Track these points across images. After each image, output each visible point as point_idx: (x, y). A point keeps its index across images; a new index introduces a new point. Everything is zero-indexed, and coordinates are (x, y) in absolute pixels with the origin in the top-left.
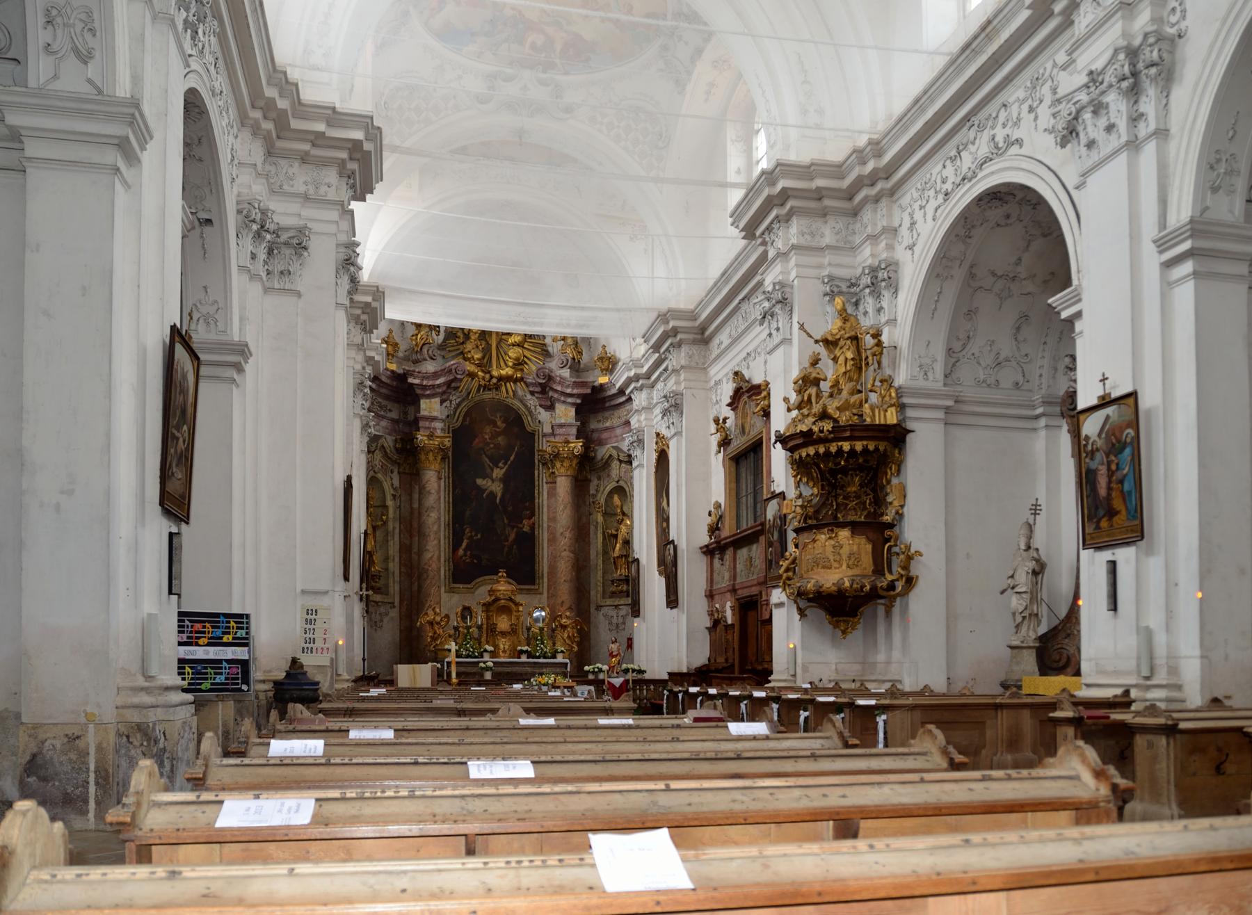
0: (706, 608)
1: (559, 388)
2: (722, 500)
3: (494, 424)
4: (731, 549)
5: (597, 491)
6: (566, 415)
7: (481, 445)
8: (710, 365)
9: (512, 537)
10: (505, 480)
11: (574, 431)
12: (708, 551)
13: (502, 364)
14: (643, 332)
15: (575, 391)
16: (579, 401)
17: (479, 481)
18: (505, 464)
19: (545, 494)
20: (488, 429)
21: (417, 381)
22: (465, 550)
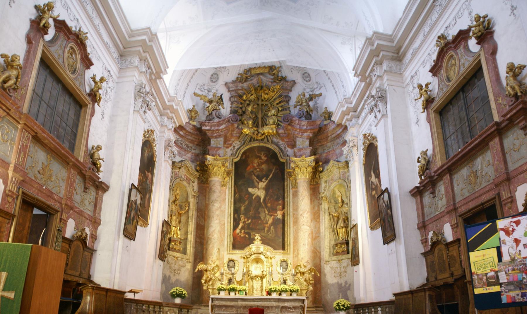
0: (419, 238)
2: (430, 147)
3: (260, 158)
4: (448, 176)
5: (325, 190)
7: (251, 170)
8: (404, 71)
9: (270, 221)
10: (267, 189)
11: (308, 151)
12: (418, 192)
14: (353, 67)
17: (250, 190)
18: (266, 179)
19: (292, 223)
21: (208, 128)
22: (241, 230)
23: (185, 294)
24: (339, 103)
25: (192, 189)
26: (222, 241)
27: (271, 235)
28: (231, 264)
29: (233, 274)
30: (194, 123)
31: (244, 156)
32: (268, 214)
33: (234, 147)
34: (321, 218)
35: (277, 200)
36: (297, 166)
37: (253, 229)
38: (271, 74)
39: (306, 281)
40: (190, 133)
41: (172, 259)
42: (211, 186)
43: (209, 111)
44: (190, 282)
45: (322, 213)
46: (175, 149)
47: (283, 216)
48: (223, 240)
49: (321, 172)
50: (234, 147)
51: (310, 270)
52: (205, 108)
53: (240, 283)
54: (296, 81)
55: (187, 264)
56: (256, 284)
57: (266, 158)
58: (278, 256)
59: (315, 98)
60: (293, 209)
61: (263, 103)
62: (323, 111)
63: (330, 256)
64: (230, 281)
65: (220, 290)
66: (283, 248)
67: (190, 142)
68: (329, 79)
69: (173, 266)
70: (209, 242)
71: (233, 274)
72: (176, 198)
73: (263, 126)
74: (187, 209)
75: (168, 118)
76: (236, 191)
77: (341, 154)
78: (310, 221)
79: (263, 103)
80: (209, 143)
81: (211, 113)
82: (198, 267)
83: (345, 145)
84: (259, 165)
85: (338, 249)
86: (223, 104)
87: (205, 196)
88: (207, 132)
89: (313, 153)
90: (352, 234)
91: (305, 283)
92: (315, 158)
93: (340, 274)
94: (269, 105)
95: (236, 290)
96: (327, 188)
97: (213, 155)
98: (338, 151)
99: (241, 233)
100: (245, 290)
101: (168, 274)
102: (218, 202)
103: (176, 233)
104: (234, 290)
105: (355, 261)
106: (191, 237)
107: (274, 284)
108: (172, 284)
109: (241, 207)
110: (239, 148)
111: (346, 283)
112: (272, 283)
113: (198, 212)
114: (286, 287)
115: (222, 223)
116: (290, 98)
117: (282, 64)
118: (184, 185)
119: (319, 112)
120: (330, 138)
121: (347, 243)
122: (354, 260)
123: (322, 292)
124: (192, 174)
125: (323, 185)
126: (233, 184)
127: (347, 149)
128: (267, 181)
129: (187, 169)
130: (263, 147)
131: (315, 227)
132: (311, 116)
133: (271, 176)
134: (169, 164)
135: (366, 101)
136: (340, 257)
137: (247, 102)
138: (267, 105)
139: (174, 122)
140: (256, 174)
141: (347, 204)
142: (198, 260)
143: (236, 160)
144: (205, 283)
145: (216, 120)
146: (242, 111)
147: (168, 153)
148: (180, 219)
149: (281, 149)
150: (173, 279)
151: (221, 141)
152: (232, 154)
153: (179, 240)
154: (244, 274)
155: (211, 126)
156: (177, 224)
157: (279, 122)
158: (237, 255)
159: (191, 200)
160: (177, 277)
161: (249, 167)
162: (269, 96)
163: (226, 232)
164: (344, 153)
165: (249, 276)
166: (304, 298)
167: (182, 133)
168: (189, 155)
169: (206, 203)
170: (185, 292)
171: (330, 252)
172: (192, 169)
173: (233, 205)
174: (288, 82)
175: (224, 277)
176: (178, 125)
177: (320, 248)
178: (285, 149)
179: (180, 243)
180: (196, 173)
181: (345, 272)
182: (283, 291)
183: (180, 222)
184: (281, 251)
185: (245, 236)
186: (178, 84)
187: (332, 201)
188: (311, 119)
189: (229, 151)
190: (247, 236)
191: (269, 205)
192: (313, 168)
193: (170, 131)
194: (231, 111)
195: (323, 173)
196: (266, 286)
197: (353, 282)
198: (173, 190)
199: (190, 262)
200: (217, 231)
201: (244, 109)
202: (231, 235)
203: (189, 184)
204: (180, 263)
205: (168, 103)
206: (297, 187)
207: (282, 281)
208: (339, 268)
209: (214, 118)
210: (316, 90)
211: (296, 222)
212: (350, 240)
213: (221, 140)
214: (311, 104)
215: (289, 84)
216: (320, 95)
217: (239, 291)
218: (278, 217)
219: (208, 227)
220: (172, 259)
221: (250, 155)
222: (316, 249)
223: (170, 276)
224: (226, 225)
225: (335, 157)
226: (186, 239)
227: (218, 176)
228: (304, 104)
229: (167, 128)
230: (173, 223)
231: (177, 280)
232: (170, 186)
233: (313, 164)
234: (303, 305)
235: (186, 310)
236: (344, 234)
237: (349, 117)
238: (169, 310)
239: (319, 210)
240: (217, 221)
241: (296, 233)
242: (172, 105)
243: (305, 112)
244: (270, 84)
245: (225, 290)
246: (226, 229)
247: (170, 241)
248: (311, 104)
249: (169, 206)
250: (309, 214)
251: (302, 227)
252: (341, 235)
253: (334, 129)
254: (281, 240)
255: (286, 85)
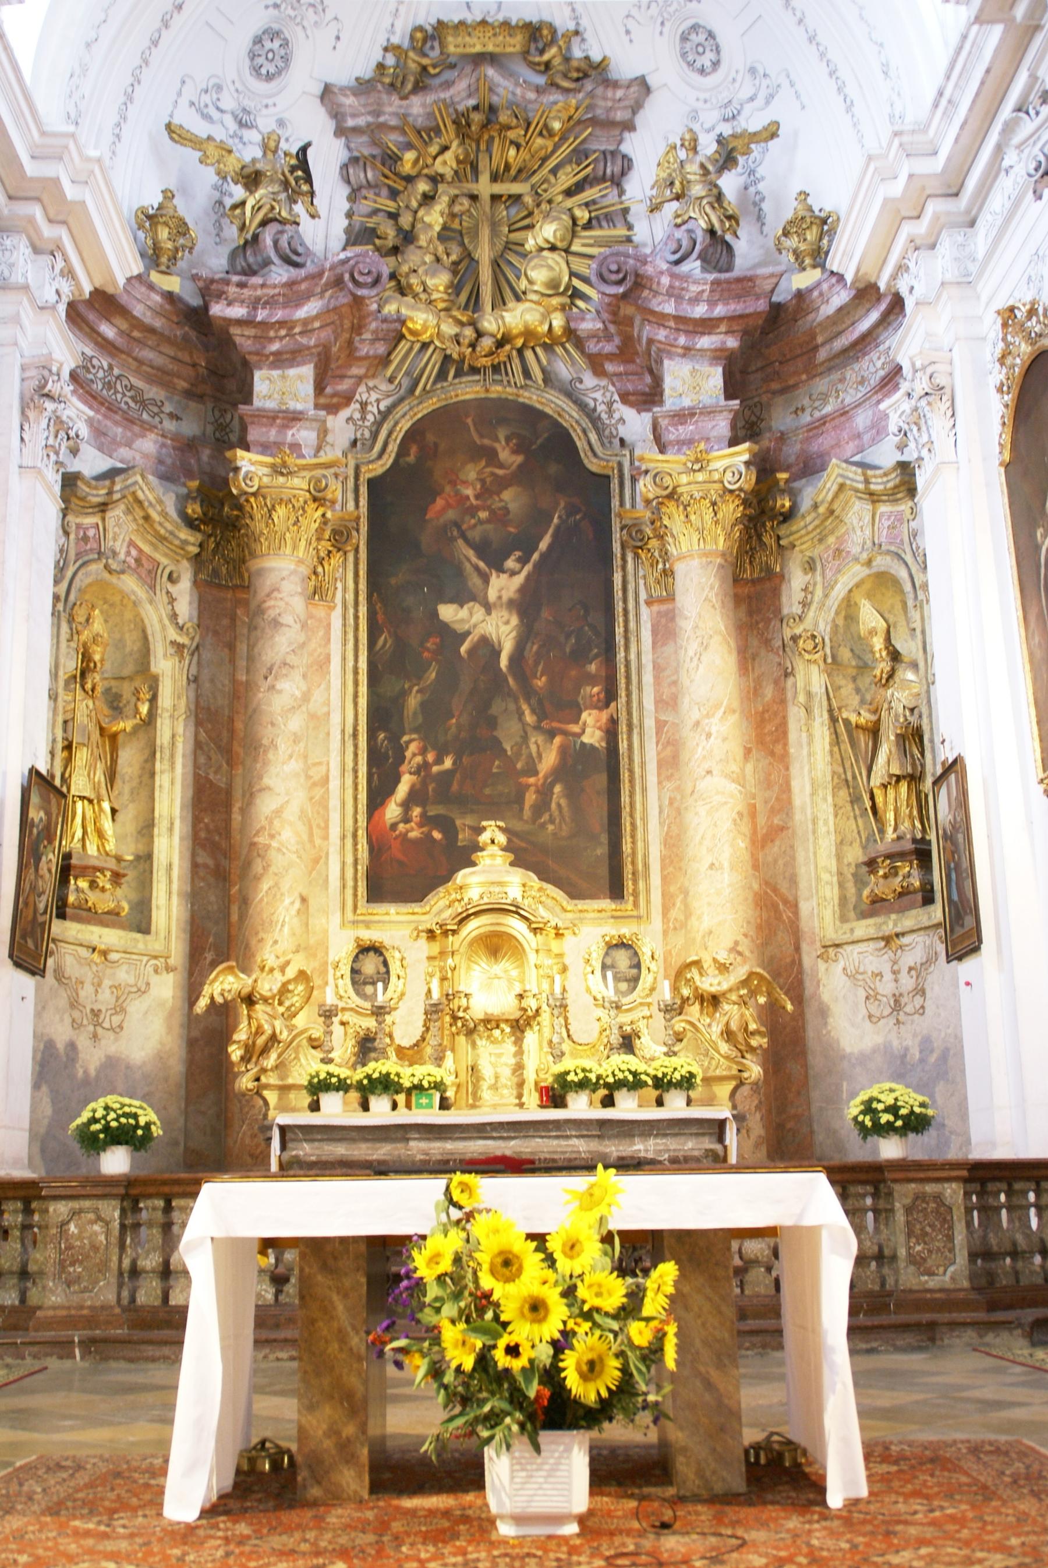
1: (669, 308)
3: (491, 456)
5: (805, 604)
6: (696, 388)
7: (451, 515)
9: (549, 760)
10: (526, 605)
11: (722, 426)
13: (508, 294)
15: (720, 311)
16: (732, 343)
17: (447, 612)
18: (523, 561)
19: (652, 767)
20: (471, 473)
21: (238, 312)
23: (147, 1126)
24: (870, 158)
25: (167, 610)
26: (316, 861)
27: (554, 828)
28: (370, 965)
29: (379, 1012)
30: (173, 284)
31: (414, 450)
32: (537, 728)
33: (364, 405)
34: (792, 736)
35: (580, 656)
36: (673, 495)
37: (463, 803)
38: (532, 65)
39: (728, 1035)
40: (151, 330)
41: (79, 959)
42: (261, 594)
43: (243, 228)
44: (177, 1066)
45: (795, 714)
46: (77, 412)
47: (611, 732)
48: (318, 860)
49: (787, 517)
50: (364, 405)
51: (745, 983)
52: (225, 211)
53: (410, 1054)
54: (651, 81)
55: (154, 979)
56: (494, 1056)
57: (519, 459)
58: (592, 926)
59: (747, 152)
60: (659, 702)
61: (499, 188)
62: (789, 215)
63: (844, 919)
64: (366, 1047)
65: (318, 1087)
66: (616, 891)
67: (150, 380)
68: (798, 97)
69: (86, 992)
70: (258, 866)
71: (379, 1012)
72: (86, 657)
73: (499, 302)
74: (144, 709)
75: (36, 250)
76: (380, 617)
77: (878, 428)
78: (739, 753)
79: (499, 188)
80: (247, 395)
81: (256, 237)
82: (207, 990)
83: (896, 387)
84: (486, 492)
85: (877, 885)
86: (312, 194)
87: (231, 647)
88: (234, 331)
89: (746, 429)
90: (943, 809)
91: (724, 1047)
92: (755, 455)
93: (897, 1004)
94: (528, 200)
95: (398, 1088)
96: (819, 593)
97: (265, 448)
98: (862, 419)
99: (406, 820)
100: (439, 1086)
101: (61, 1033)
102: (297, 675)
103: (96, 832)
104: (386, 1084)
105: (962, 937)
106: (170, 849)
107: (574, 1055)
108: (86, 1082)
109: (404, 694)
110: (390, 410)
111: (926, 1044)
112: (566, 1046)
113: (198, 723)
114: (633, 1063)
115: (317, 773)
116: (627, 164)
117: (584, 22)
118: (124, 595)
119: (769, 219)
120: (822, 354)
121: (922, 854)
122: (959, 931)
123: (815, 1095)
124: (162, 539)
125: (797, 580)
126: (363, 586)
127: (906, 406)
128: (528, 567)
129: (139, 513)
130: (502, 403)
131: (767, 783)
132: (729, 247)
133: (543, 545)
134: (49, 488)
135: (1009, 128)
136: (890, 924)
137: (423, 186)
138: (517, 198)
139: (69, 273)
140: (475, 535)
141: (914, 666)
142: (209, 956)
143: (379, 468)
144: (246, 1059)
145: (280, 274)
146: (399, 229)
147: (39, 432)
148: (114, 761)
149: (590, 413)
150: (91, 1059)
151: (300, 378)
152: (354, 443)
153: (112, 864)
154: (433, 1011)
155: (255, 304)
156: (96, 788)
157: (576, 282)
158: (396, 925)
159: (167, 667)
160: (110, 1046)
161: (440, 502)
162: (524, 154)
163: (335, 817)
164: (892, 428)
165: (455, 1018)
166: (724, 1112)
167: (108, 331)
168: (149, 444)
169: (234, 681)
170: (147, 1115)
171: (843, 900)
172: (164, 514)
173: (363, 689)
174: (615, 85)
175: (337, 1029)
176: (87, 289)
177: (793, 881)
178: (610, 412)
179: (117, 877)
180: (185, 534)
181: (920, 991)
182: (620, 1084)
183: (112, 775)
184: (606, 904)
185: (428, 836)
186: (85, 70)
187: (845, 654)
188: (729, 268)
189: (341, 427)
190: (437, 835)
191: (541, 682)
192: (746, 503)
193: (46, 315)
194: (348, 231)
195: (796, 525)
196: (539, 1065)
197: (959, 1039)
198: (71, 620)
199: (168, 969)
200: (292, 813)
201: (405, 221)
202: (362, 833)
203: (153, 587)
204: (123, 975)
205: (31, 169)
206: (671, 598)
207: (616, 1039)
208: (888, 976)
209: (267, 263)
210: (748, 109)
211: (671, 763)
212: (932, 836)
213: (303, 375)
214: (729, 183)
215: (619, 93)
216: (771, 132)
217: (409, 1092)
218: (586, 739)
219: (250, 796)
220: (79, 959)
221: (443, 446)
222: (775, 890)
223: (72, 1046)
224: (334, 784)
225: (850, 448)
226: (146, 858)
227: (295, 547)
228: (697, 190)
229: (32, 300)
230: (79, 784)
231: (111, 1063)
232: (56, 598)
233: (748, 481)
234: (718, 1147)
235: (161, 1203)
236: (904, 810)
237: (920, 228)
238: (75, 1213)
239: (783, 702)
240: (294, 765)
241: (676, 813)
242: (56, 181)
243: (700, 236)
244: (531, 95)
245: (342, 1086)
246: (334, 803)
247: (66, 870)
248: (729, 183)
249: (53, 697)
250: (733, 719)
251: (702, 785)
252: (890, 816)
253: (840, 309)
254: (602, 850)
255: (605, 103)
